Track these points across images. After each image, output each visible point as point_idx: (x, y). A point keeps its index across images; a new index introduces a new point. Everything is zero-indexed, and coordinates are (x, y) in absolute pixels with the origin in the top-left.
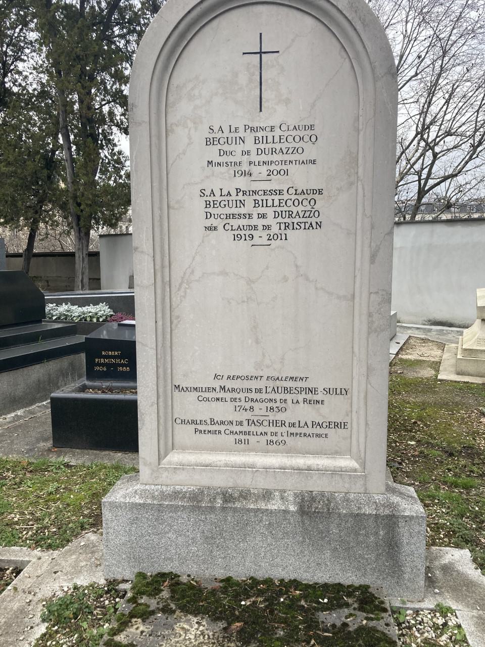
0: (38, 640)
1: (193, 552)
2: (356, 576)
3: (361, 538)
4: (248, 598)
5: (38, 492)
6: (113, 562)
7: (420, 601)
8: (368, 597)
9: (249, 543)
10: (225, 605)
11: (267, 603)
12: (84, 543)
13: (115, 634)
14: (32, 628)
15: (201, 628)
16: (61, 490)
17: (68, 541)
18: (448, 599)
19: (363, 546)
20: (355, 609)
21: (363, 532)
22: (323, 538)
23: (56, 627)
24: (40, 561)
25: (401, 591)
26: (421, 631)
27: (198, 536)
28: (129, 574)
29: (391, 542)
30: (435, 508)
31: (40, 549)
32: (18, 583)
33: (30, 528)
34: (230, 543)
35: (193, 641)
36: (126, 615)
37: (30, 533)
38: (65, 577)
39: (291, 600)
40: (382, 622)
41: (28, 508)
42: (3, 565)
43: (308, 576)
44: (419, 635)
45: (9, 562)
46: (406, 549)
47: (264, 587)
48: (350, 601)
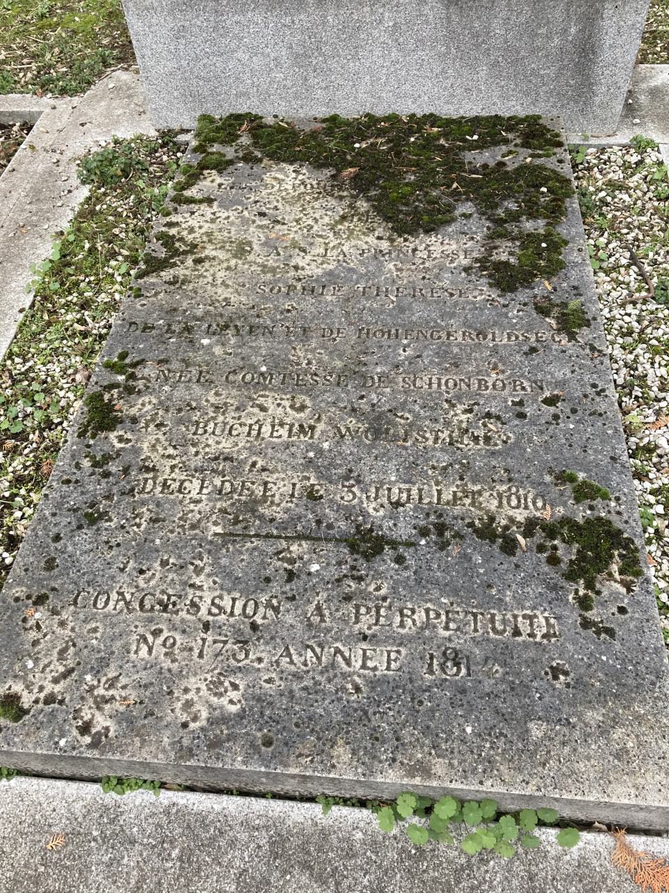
0: (83, 205)
1: (279, 82)
2: (523, 104)
3: (539, 42)
4: (363, 140)
5: (23, 15)
6: (162, 103)
7: (609, 136)
8: (537, 130)
9: (362, 60)
10: (331, 150)
11: (392, 145)
12: (113, 85)
13: (183, 189)
14: (70, 191)
15: (301, 177)
16: (58, 11)
17: (89, 83)
18: (651, 130)
19: (540, 54)
20: (516, 145)
21: (543, 31)
22: (478, 46)
23: (103, 190)
24: (56, 111)
25: (585, 122)
26: (604, 172)
27: (283, 53)
28: (188, 120)
29: (585, 45)
30: (655, 9)
31: (50, 95)
32: (34, 140)
33: (28, 68)
34: (333, 64)
35: (291, 191)
36: (194, 167)
37: (29, 75)
38: (99, 130)
39: (426, 139)
40: (554, 159)
41: (14, 39)
42: (4, 120)
43: (447, 111)
44: (601, 177)
45: (12, 114)
46: (606, 56)
47: (386, 125)
48: (510, 136)
